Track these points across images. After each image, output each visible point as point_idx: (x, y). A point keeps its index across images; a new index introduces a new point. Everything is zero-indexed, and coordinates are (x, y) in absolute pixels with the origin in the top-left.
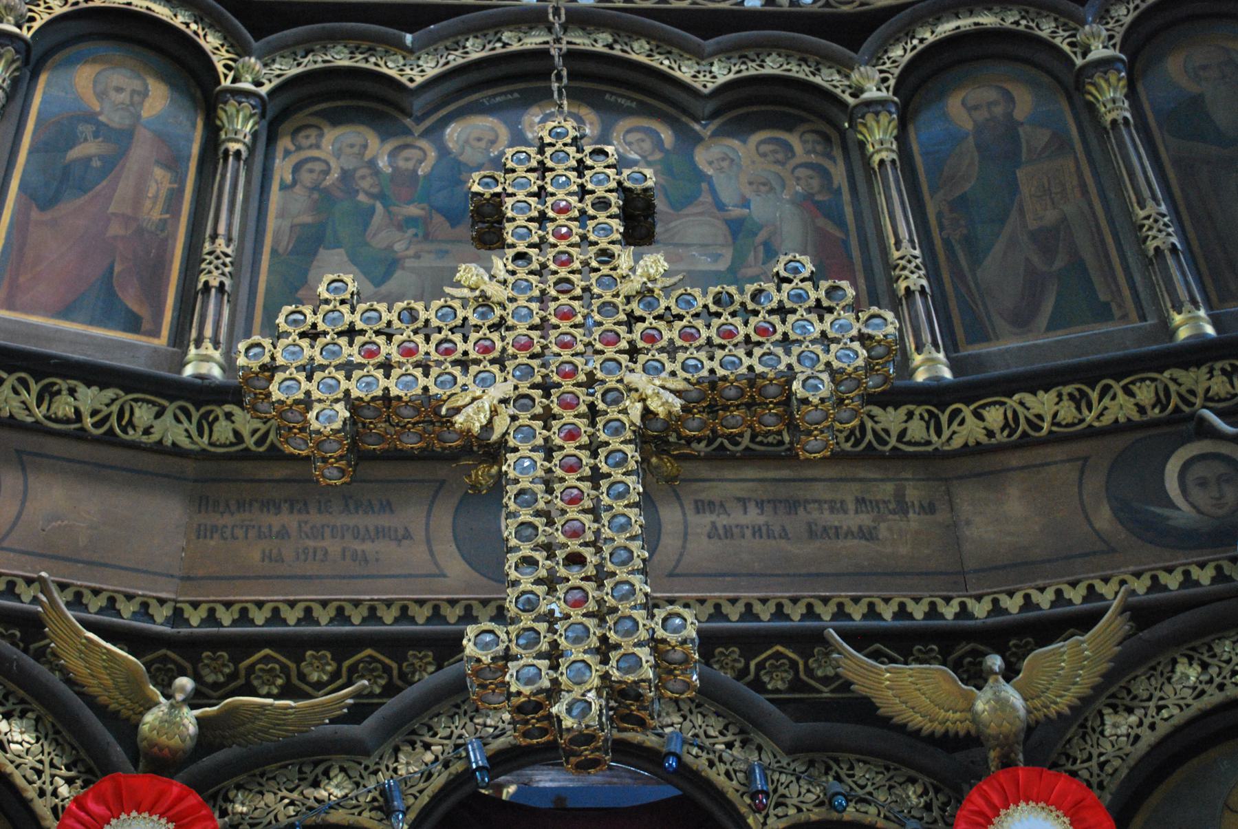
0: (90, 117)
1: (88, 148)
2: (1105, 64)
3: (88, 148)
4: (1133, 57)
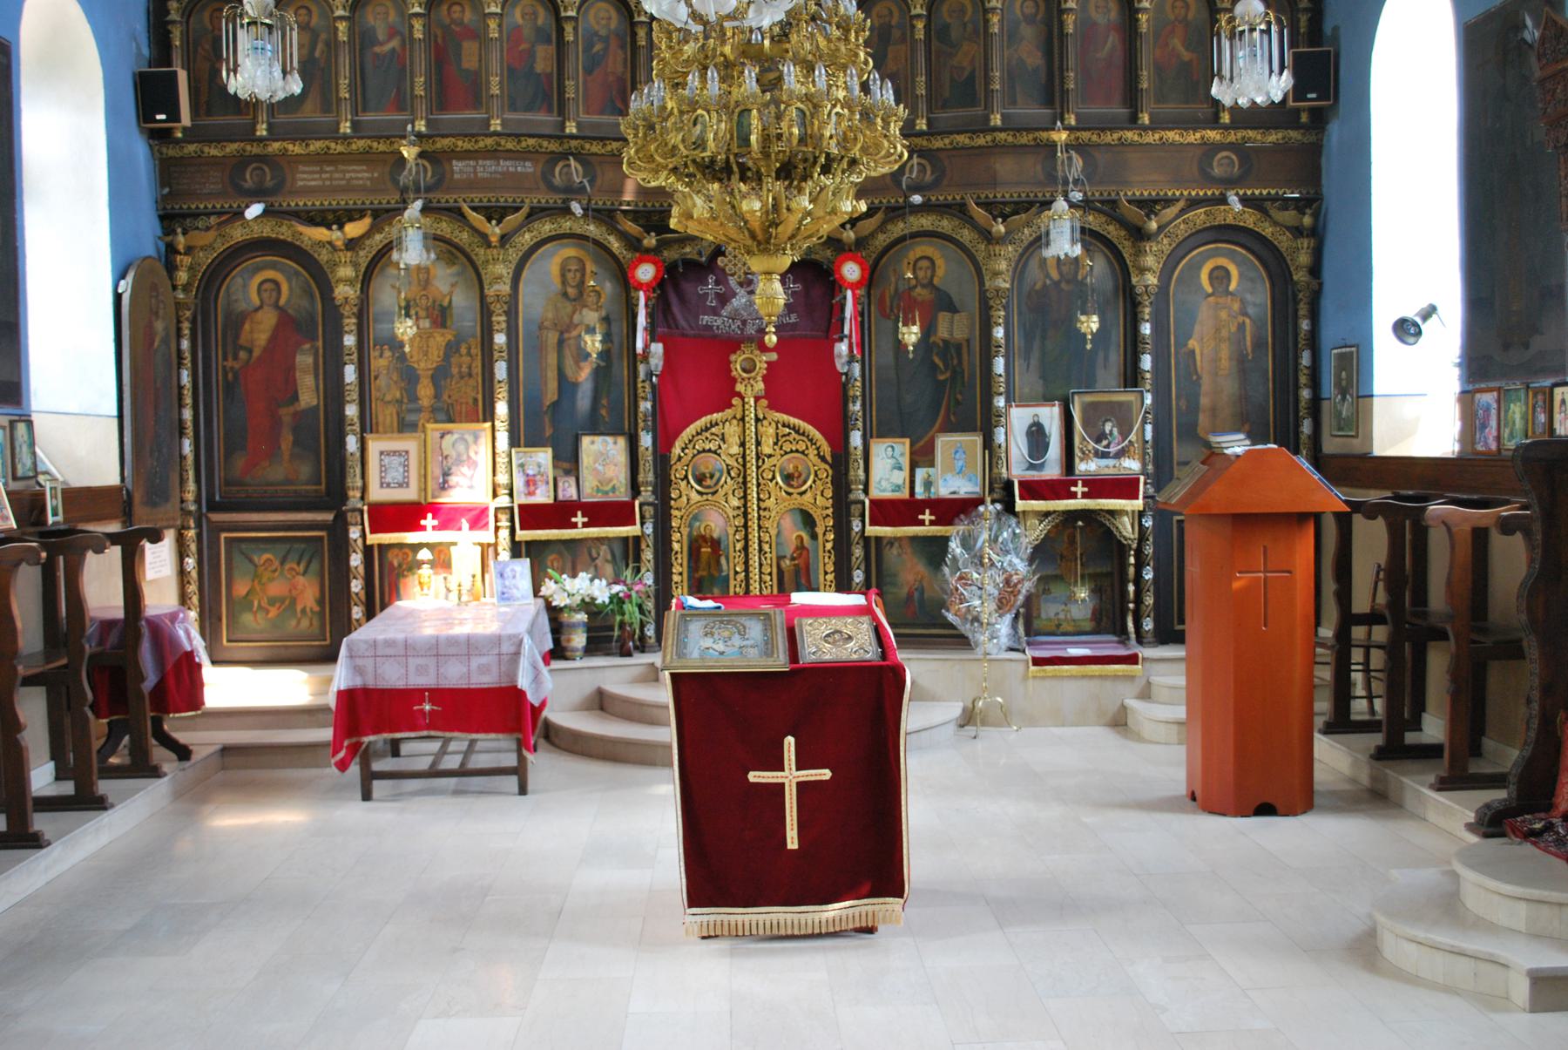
0: (596, 34)
1: (598, 47)
2: (919, 16)
3: (598, 47)
4: (929, 10)
